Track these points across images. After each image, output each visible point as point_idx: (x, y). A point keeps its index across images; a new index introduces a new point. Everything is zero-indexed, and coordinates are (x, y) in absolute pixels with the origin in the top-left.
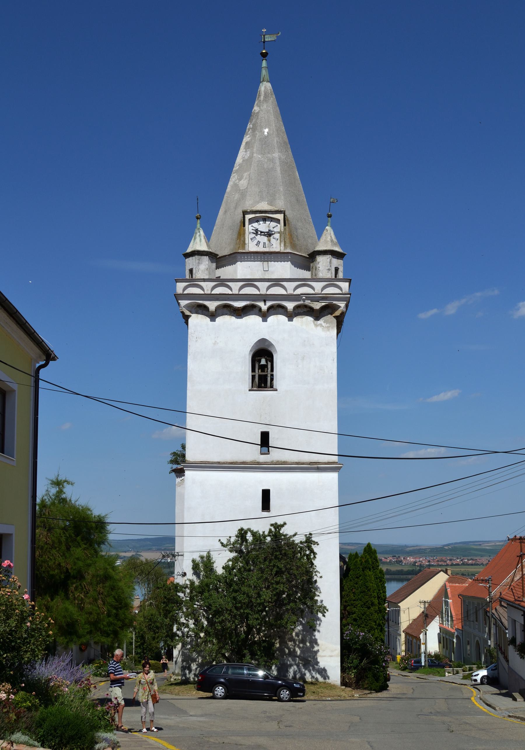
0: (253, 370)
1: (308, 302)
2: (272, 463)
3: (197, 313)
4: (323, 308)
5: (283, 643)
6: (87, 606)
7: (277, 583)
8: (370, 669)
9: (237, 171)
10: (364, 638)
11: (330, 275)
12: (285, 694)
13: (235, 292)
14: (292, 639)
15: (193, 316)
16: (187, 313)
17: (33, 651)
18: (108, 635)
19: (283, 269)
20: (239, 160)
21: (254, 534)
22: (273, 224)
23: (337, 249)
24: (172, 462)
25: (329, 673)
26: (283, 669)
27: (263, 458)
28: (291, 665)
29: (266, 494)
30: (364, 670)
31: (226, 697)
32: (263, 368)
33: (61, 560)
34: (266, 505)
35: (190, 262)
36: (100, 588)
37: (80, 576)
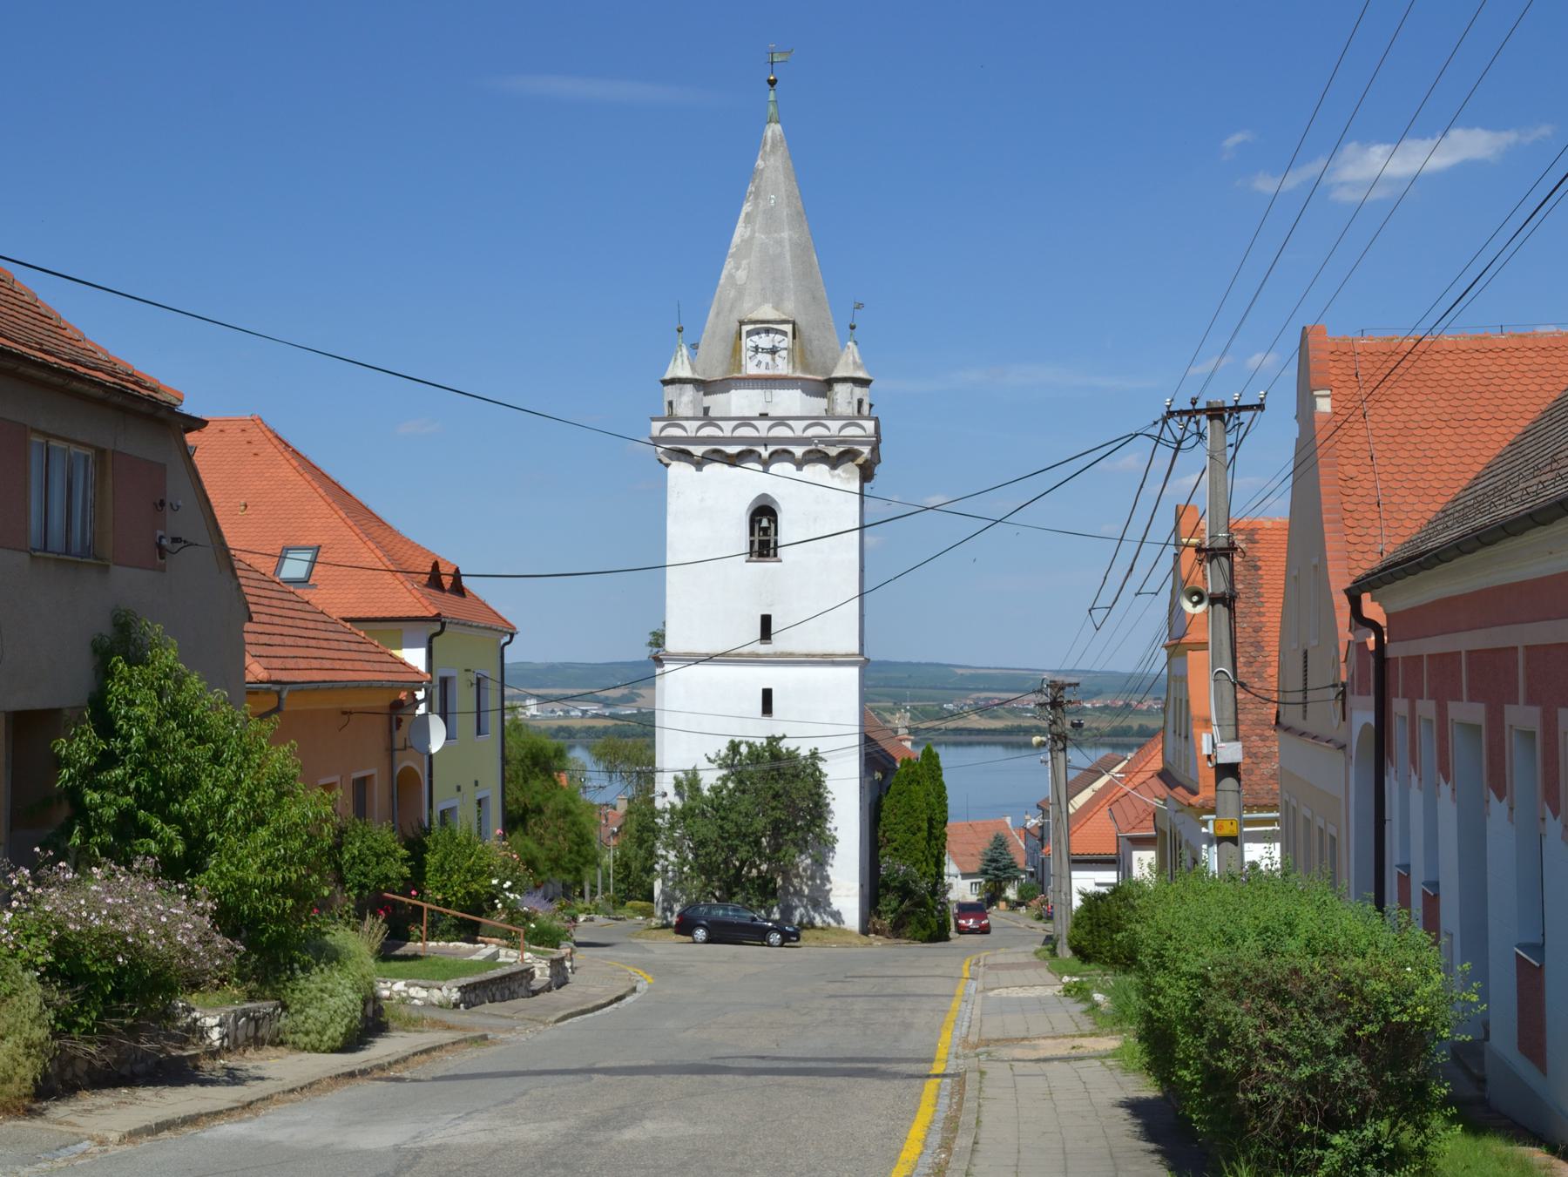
0: (752, 534)
1: (821, 447)
2: (775, 655)
3: (679, 460)
4: (842, 454)
5: (786, 879)
6: (548, 842)
7: (773, 809)
8: (914, 913)
9: (733, 255)
10: (905, 874)
11: (851, 410)
12: (775, 938)
13: (727, 433)
14: (798, 875)
15: (674, 464)
16: (666, 460)
17: (1284, 1021)
18: (570, 872)
19: (791, 401)
20: (736, 239)
21: (750, 746)
22: (779, 337)
23: (861, 374)
24: (651, 644)
25: (844, 917)
26: (787, 911)
27: (763, 649)
28: (796, 907)
29: (767, 695)
30: (906, 913)
31: (708, 941)
32: (765, 530)
33: (518, 794)
34: (767, 707)
35: (670, 392)
36: (560, 822)
37: (539, 811)
